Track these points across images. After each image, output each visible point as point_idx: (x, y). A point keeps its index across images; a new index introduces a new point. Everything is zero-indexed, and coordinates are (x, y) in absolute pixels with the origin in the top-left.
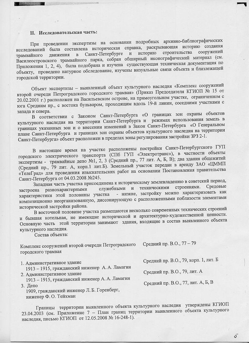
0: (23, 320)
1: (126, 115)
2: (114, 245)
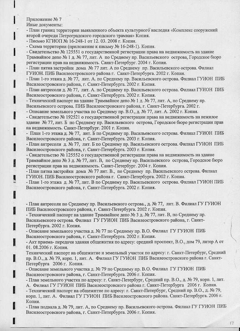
0: (65, 63)
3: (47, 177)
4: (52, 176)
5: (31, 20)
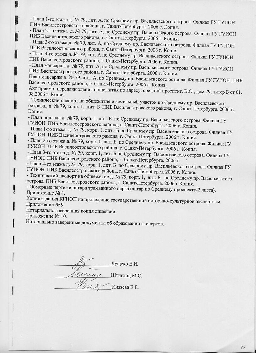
1: (152, 126)
2: (184, 45)
3: (49, 147)
4: (55, 123)
5: (31, 204)
